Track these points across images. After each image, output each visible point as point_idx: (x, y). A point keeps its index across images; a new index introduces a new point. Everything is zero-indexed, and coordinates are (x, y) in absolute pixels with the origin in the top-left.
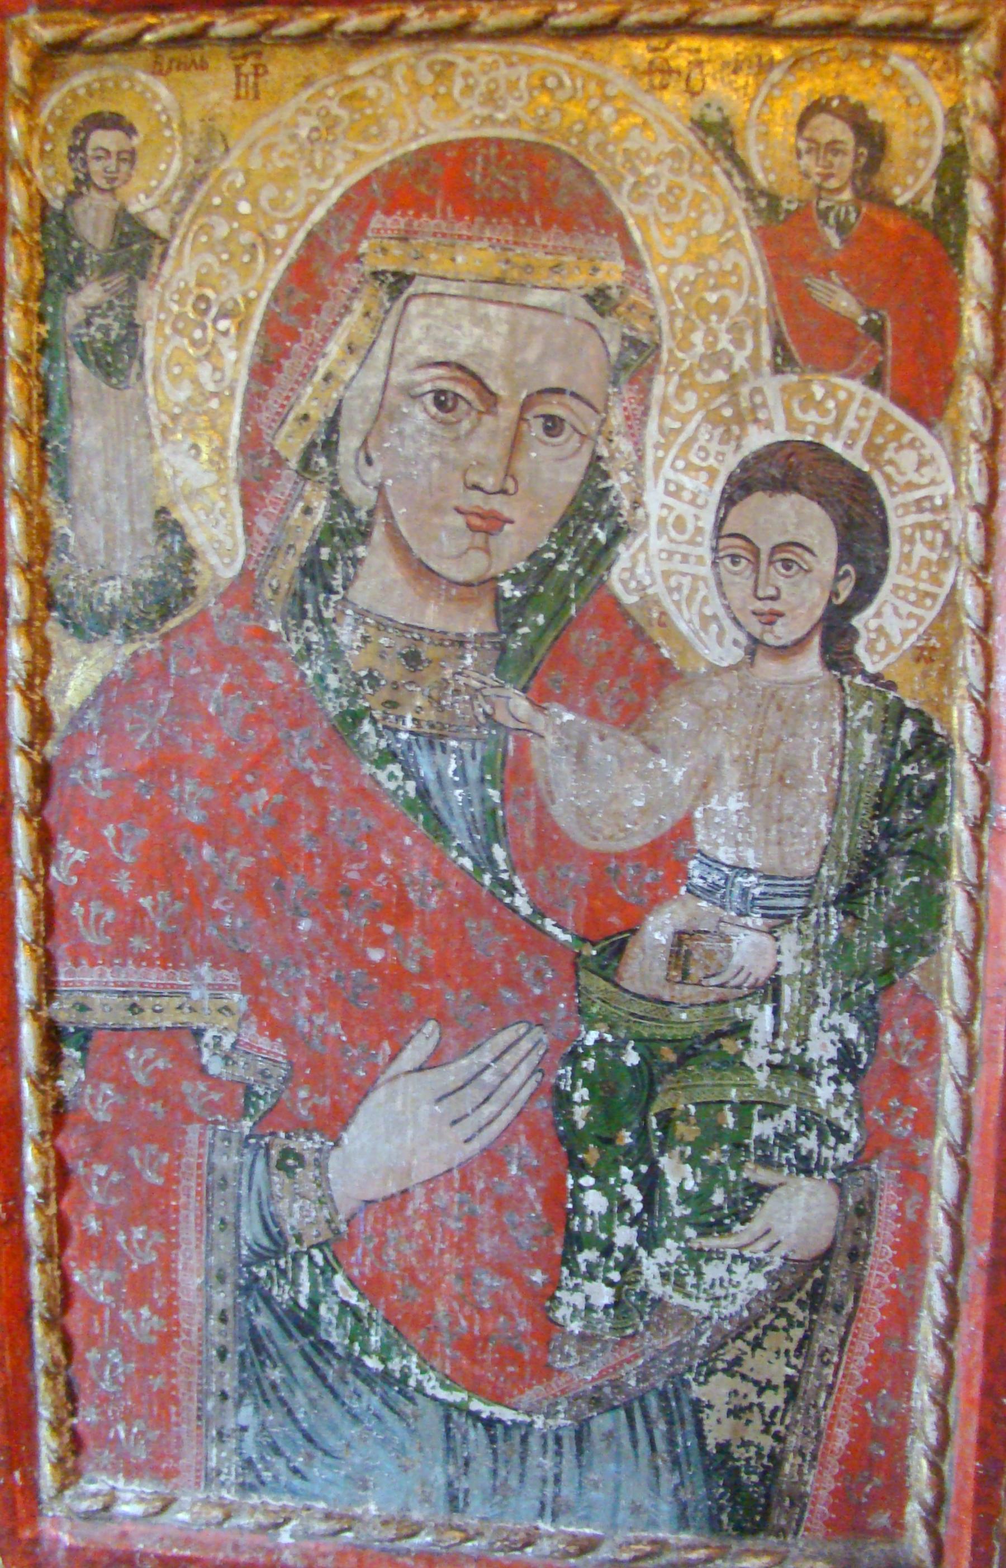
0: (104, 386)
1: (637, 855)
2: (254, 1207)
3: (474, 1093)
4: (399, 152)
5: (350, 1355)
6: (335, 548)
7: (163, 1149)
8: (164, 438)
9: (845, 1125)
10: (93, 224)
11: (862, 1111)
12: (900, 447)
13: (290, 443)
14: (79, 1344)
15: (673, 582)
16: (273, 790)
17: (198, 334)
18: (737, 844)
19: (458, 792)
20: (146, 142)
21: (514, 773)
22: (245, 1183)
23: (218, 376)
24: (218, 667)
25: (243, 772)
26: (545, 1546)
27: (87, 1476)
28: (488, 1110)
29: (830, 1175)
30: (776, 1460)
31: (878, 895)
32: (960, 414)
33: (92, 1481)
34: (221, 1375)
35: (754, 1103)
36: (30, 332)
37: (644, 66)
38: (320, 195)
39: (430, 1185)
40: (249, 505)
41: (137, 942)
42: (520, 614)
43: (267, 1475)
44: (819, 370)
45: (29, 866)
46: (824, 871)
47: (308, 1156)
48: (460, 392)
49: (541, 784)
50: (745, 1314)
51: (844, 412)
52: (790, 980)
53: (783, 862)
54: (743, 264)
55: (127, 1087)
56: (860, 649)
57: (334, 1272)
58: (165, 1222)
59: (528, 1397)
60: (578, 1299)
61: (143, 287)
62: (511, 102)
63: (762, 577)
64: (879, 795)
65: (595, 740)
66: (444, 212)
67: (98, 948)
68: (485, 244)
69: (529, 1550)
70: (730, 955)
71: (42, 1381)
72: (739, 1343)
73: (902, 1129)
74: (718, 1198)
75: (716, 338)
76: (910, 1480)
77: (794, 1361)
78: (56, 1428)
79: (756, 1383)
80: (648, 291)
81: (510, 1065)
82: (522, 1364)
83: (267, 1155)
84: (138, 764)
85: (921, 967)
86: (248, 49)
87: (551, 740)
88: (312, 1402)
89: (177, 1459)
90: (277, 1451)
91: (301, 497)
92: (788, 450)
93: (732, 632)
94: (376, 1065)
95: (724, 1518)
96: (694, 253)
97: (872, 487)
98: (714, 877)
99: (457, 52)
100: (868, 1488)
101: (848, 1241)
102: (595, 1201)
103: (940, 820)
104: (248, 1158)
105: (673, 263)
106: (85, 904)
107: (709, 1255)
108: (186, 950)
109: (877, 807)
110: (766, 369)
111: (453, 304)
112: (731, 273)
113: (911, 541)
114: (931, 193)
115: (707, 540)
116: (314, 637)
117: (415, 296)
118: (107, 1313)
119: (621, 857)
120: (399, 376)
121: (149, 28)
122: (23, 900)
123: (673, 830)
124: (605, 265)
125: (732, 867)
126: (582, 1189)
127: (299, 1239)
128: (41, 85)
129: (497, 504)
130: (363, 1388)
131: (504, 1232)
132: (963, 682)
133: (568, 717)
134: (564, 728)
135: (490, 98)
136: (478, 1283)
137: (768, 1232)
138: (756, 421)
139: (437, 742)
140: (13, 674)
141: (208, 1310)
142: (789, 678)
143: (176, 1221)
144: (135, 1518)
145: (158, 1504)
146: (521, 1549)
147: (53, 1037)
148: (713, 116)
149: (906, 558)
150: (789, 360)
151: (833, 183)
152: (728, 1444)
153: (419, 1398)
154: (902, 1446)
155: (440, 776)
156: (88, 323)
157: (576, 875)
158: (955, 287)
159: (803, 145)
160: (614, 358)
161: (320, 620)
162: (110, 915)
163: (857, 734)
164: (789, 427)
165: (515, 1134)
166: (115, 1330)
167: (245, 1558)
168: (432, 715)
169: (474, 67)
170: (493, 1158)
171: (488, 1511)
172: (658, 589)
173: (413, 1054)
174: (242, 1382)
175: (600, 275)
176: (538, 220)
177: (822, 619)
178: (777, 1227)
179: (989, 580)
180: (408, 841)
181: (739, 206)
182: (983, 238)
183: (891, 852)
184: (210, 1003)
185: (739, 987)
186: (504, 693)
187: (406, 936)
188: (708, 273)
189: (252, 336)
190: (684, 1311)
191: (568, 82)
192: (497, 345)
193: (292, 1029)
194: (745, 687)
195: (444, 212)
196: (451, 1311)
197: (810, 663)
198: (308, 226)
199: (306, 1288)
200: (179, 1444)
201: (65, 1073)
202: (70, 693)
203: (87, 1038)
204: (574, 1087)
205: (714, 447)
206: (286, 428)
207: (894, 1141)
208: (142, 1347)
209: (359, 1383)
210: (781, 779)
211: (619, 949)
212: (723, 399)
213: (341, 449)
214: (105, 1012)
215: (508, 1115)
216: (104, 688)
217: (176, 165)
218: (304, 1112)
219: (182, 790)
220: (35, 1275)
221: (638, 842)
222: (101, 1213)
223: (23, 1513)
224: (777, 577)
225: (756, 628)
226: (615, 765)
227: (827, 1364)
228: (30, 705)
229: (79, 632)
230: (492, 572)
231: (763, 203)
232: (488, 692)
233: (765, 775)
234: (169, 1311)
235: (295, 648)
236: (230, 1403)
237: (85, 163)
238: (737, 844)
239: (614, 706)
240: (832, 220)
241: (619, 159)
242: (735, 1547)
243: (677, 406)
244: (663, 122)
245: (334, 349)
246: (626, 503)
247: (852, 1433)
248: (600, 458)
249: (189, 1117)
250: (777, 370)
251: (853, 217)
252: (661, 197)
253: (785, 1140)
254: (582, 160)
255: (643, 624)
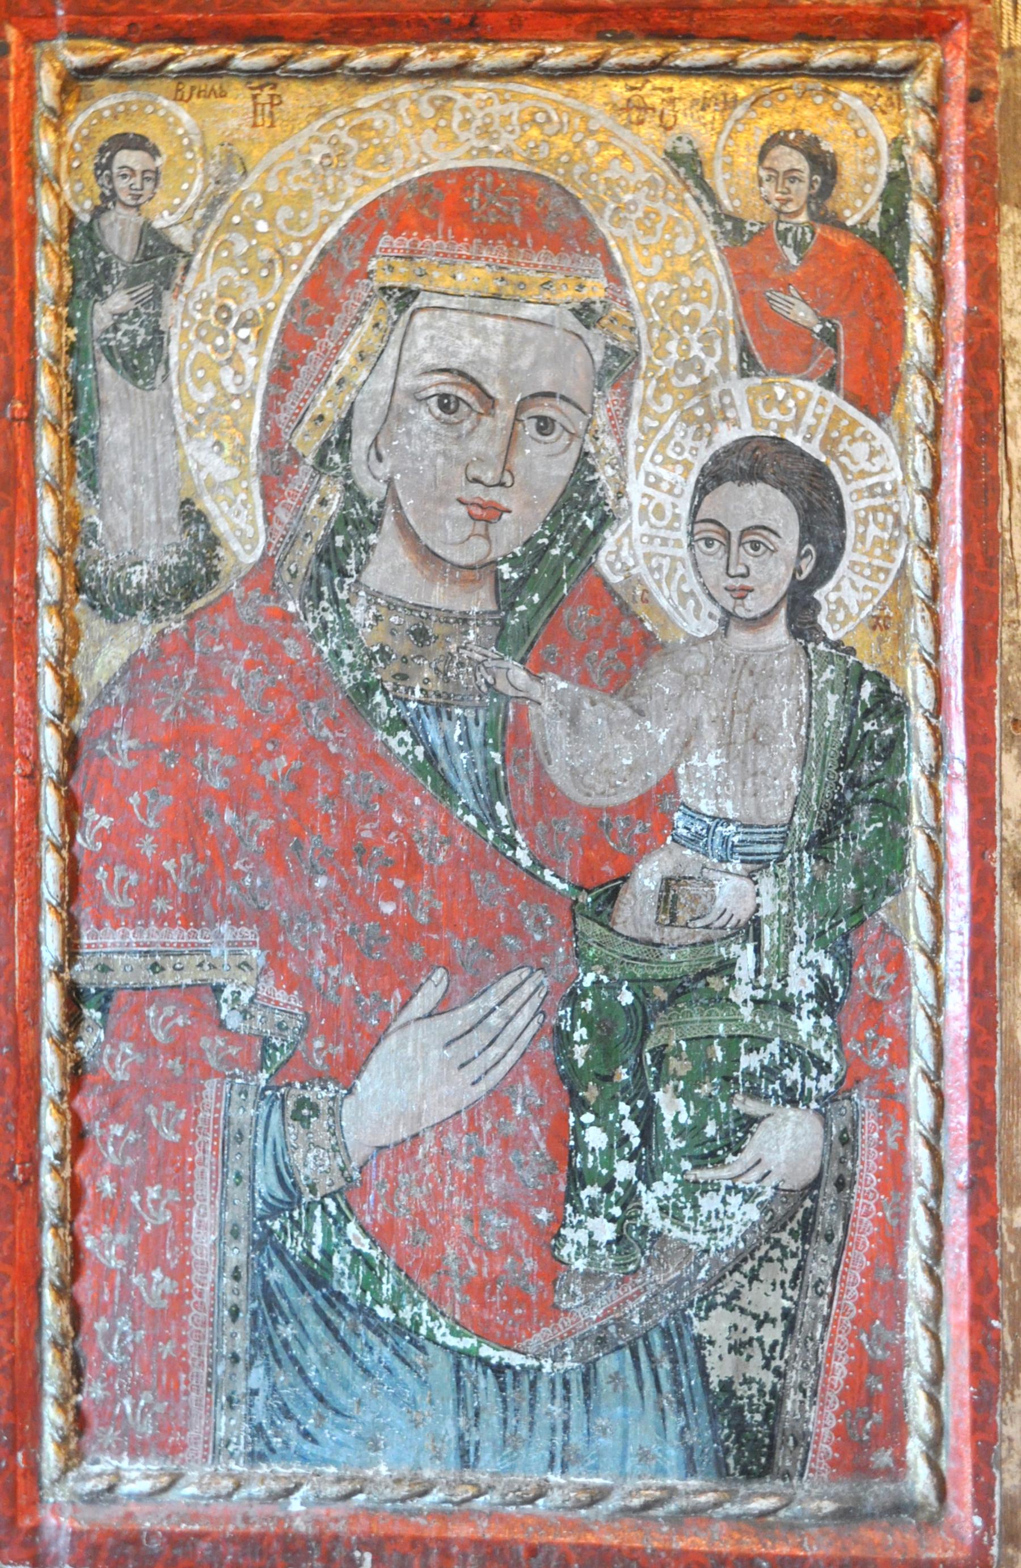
0: (131, 387)
1: (626, 809)
2: (269, 1159)
3: (480, 1038)
4: (404, 179)
5: (362, 1306)
6: (349, 536)
7: (179, 1107)
8: (190, 436)
9: (826, 1056)
10: (119, 235)
11: (841, 1043)
12: (854, 440)
13: (306, 442)
14: (87, 1313)
15: (654, 563)
16: (290, 756)
17: (220, 341)
18: (717, 796)
19: (463, 755)
20: (169, 161)
21: (515, 738)
22: (260, 1135)
23: (239, 379)
24: (240, 646)
25: (264, 740)
26: (556, 1497)
27: (90, 1458)
28: (494, 1052)
29: (814, 1105)
30: (778, 1396)
31: (846, 840)
32: (907, 409)
33: (96, 1462)
34: (233, 1336)
35: (740, 1037)
36: (59, 335)
37: (622, 103)
38: (333, 217)
39: (440, 1128)
40: (268, 499)
41: (160, 904)
42: (519, 594)
43: (277, 1442)
44: (779, 374)
45: (57, 833)
46: (796, 819)
47: (323, 1106)
48: (461, 396)
49: (539, 747)
50: (741, 1245)
51: (803, 410)
52: (769, 919)
53: (758, 810)
54: (713, 280)
55: (147, 1045)
56: (822, 620)
57: (348, 1220)
58: (181, 1182)
59: (536, 1340)
60: (582, 1236)
61: (167, 297)
62: (505, 135)
63: (733, 557)
64: (844, 750)
65: (587, 705)
66: (445, 233)
67: (122, 911)
68: (482, 263)
69: (540, 1502)
70: (714, 899)
71: (49, 1355)
72: (737, 1276)
73: (878, 1060)
74: (711, 1130)
75: (689, 346)
76: (910, 1416)
77: (789, 1292)
78: (62, 1403)
79: (755, 1316)
80: (628, 305)
81: (515, 1008)
82: (529, 1306)
83: (283, 1107)
84: (162, 734)
85: (889, 907)
86: (263, 81)
87: (547, 706)
88: (324, 1360)
89: (184, 1431)
90: (288, 1414)
91: (316, 490)
92: (754, 445)
93: (708, 606)
94: (388, 1013)
95: (731, 1461)
96: (670, 271)
97: (830, 476)
98: (697, 827)
99: (456, 89)
100: (868, 1425)
101: (834, 1171)
102: (596, 1138)
103: (899, 771)
104: (264, 1109)
105: (650, 280)
106: (109, 868)
107: (707, 1187)
108: (207, 909)
109: (841, 760)
110: (734, 374)
111: (454, 317)
112: (701, 289)
113: (865, 522)
114: (878, 214)
115: (684, 526)
116: (330, 617)
117: (420, 309)
118: (118, 1279)
119: (612, 811)
120: (406, 381)
121: (173, 58)
122: (51, 865)
123: (659, 784)
124: (589, 282)
125: (714, 818)
126: (583, 1126)
127: (313, 1190)
128: (69, 107)
129: (495, 495)
130: (375, 1340)
131: (510, 1171)
132: (915, 646)
133: (562, 685)
134: (559, 695)
135: (485, 131)
136: (487, 1225)
137: (759, 1161)
138: (725, 419)
139: (443, 711)
140: (43, 651)
141: (221, 1269)
142: (761, 646)
143: (192, 1178)
144: (140, 1497)
145: (165, 1480)
146: (532, 1501)
147: (74, 998)
148: (684, 148)
149: (862, 538)
150: (754, 365)
151: (791, 207)
152: (731, 1381)
153: (430, 1347)
154: (898, 1381)
155: (446, 742)
156: (116, 329)
157: (572, 828)
158: (901, 296)
159: (764, 174)
160: (598, 366)
161: (335, 601)
162: (133, 878)
163: (822, 694)
164: (754, 424)
165: (520, 1074)
166: (125, 1296)
167: (255, 1529)
168: (439, 686)
169: (470, 103)
170: (499, 1099)
171: (498, 1465)
172: (641, 570)
173: (421, 1003)
174: (253, 1342)
175: (585, 291)
176: (529, 241)
177: (788, 592)
178: (767, 1157)
179: (936, 555)
180: (417, 801)
181: (708, 228)
182: (924, 253)
183: (856, 800)
184: (228, 957)
185: (723, 928)
186: (504, 665)
187: (416, 889)
188: (681, 289)
189: (271, 344)
190: (683, 1244)
191: (555, 118)
192: (494, 353)
193: (309, 981)
194: (720, 654)
195: (445, 233)
196: (461, 1252)
197: (778, 633)
198: (321, 244)
199: (318, 1240)
200: (187, 1417)
201: (85, 1035)
202: (97, 670)
203: (108, 999)
204: (573, 1027)
205: (688, 443)
206: (303, 427)
207: (872, 1072)
208: (153, 1312)
209: (370, 1334)
210: (755, 737)
211: (613, 896)
212: (696, 400)
213: (354, 446)
214: (127, 971)
215: (513, 1056)
216: (132, 663)
217: (198, 185)
218: (319, 1062)
219: (206, 757)
220: (49, 1241)
221: (627, 797)
222: (116, 1174)
223: (23, 1500)
224: (747, 557)
225: (729, 603)
226: (606, 729)
227: (821, 1295)
228: (60, 680)
229: (107, 613)
230: (492, 556)
231: (729, 225)
232: (489, 664)
233: (740, 735)
234: (181, 1272)
235: (312, 626)
236: (241, 1365)
237: (111, 180)
238: (717, 796)
239: (603, 675)
240: (790, 241)
241: (601, 187)
242: (743, 1491)
243: (655, 408)
244: (640, 154)
245: (347, 356)
246: (611, 494)
247: (850, 1366)
248: (587, 454)
249: (208, 1072)
250: (743, 374)
251: (808, 236)
252: (639, 221)
253: (771, 1072)
254: (569, 188)
255: (627, 599)
